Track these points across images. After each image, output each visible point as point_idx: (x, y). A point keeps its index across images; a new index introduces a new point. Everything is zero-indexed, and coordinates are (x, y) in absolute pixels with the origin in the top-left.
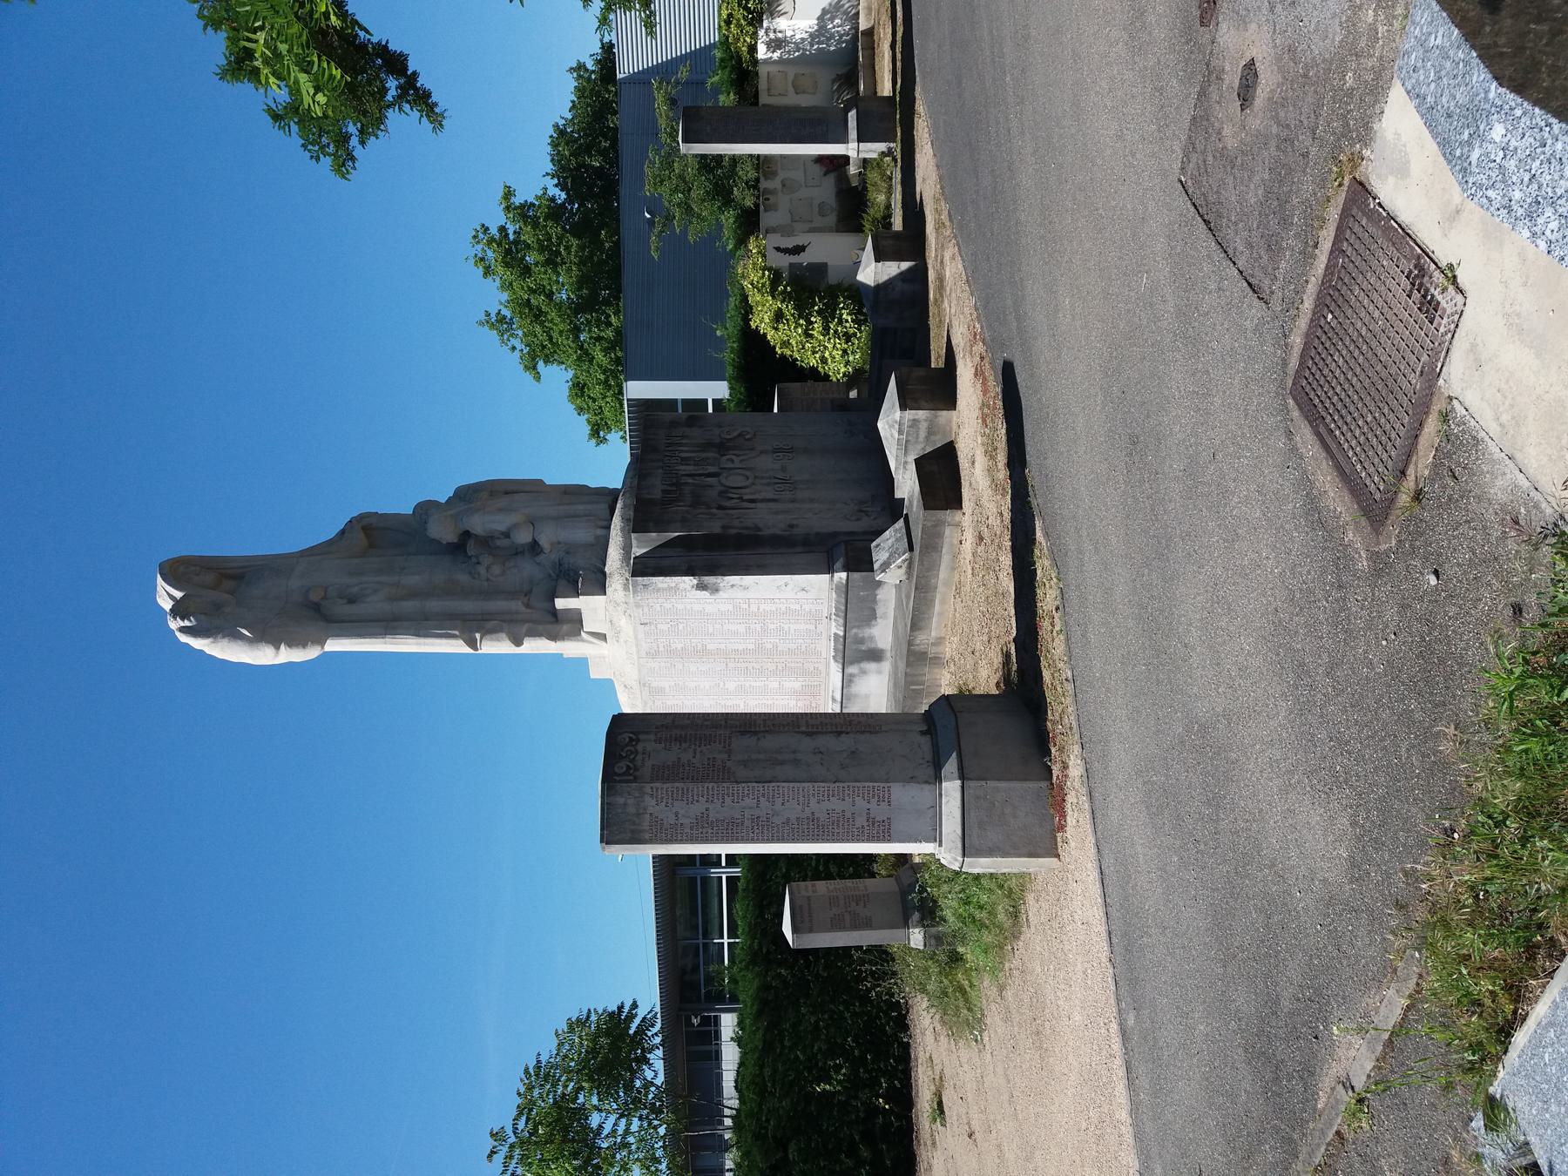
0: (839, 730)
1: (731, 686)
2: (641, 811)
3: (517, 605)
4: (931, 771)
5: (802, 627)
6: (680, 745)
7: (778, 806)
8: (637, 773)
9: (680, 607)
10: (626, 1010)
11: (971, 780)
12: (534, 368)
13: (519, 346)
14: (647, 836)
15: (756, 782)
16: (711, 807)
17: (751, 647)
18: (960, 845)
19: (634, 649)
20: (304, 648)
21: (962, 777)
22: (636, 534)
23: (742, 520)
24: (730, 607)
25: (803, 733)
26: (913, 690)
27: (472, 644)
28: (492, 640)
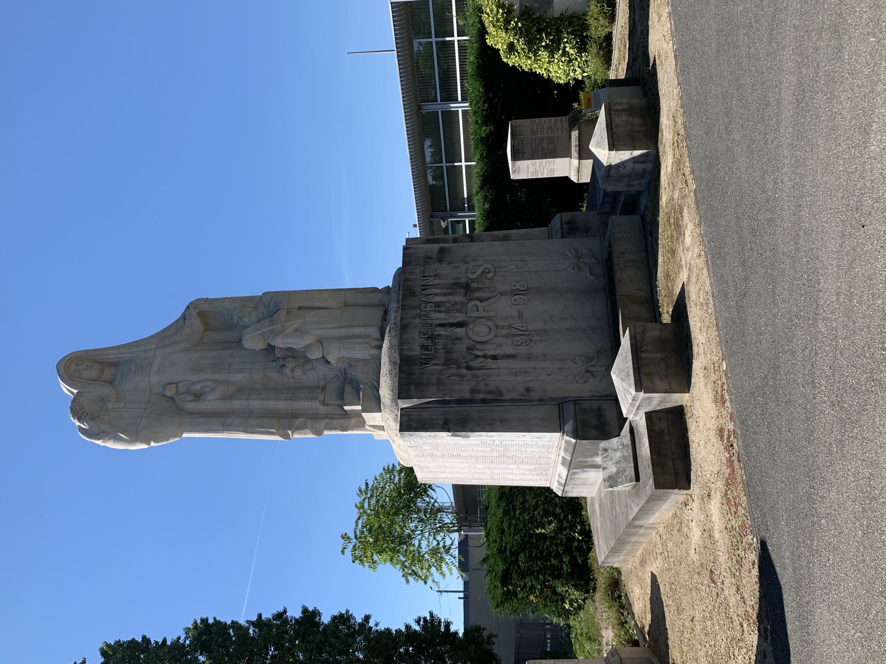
3: (315, 406)
22: (400, 400)
23: (487, 382)
27: (286, 436)
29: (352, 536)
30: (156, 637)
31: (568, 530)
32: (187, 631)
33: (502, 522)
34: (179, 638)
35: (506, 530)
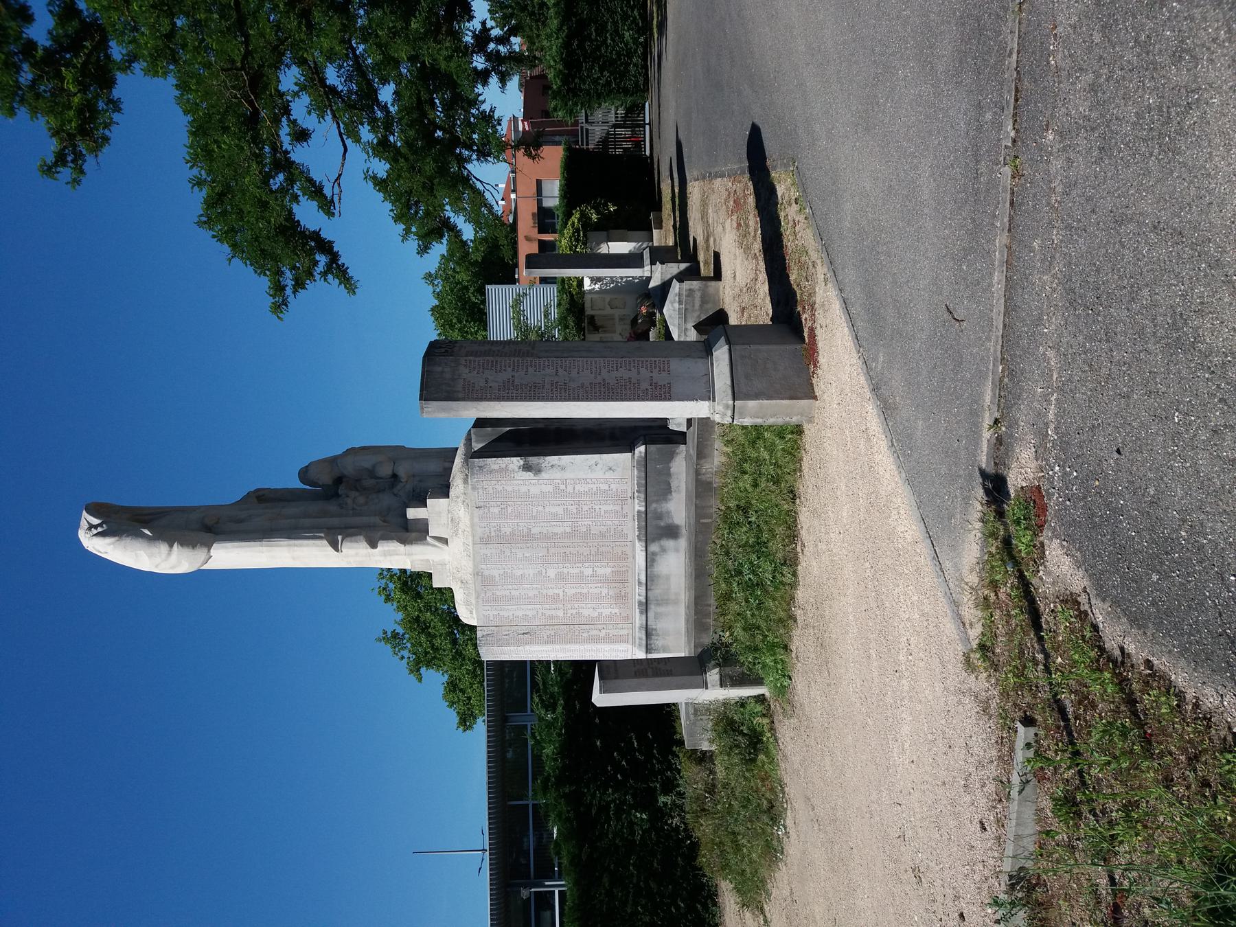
1: (552, 573)
2: (456, 377)
5: (610, 508)
7: (574, 374)
9: (509, 488)
12: (418, 670)
13: (406, 653)
14: (460, 395)
16: (516, 375)
17: (568, 530)
18: (730, 392)
19: (470, 538)
20: (193, 548)
24: (550, 488)
28: (351, 541)
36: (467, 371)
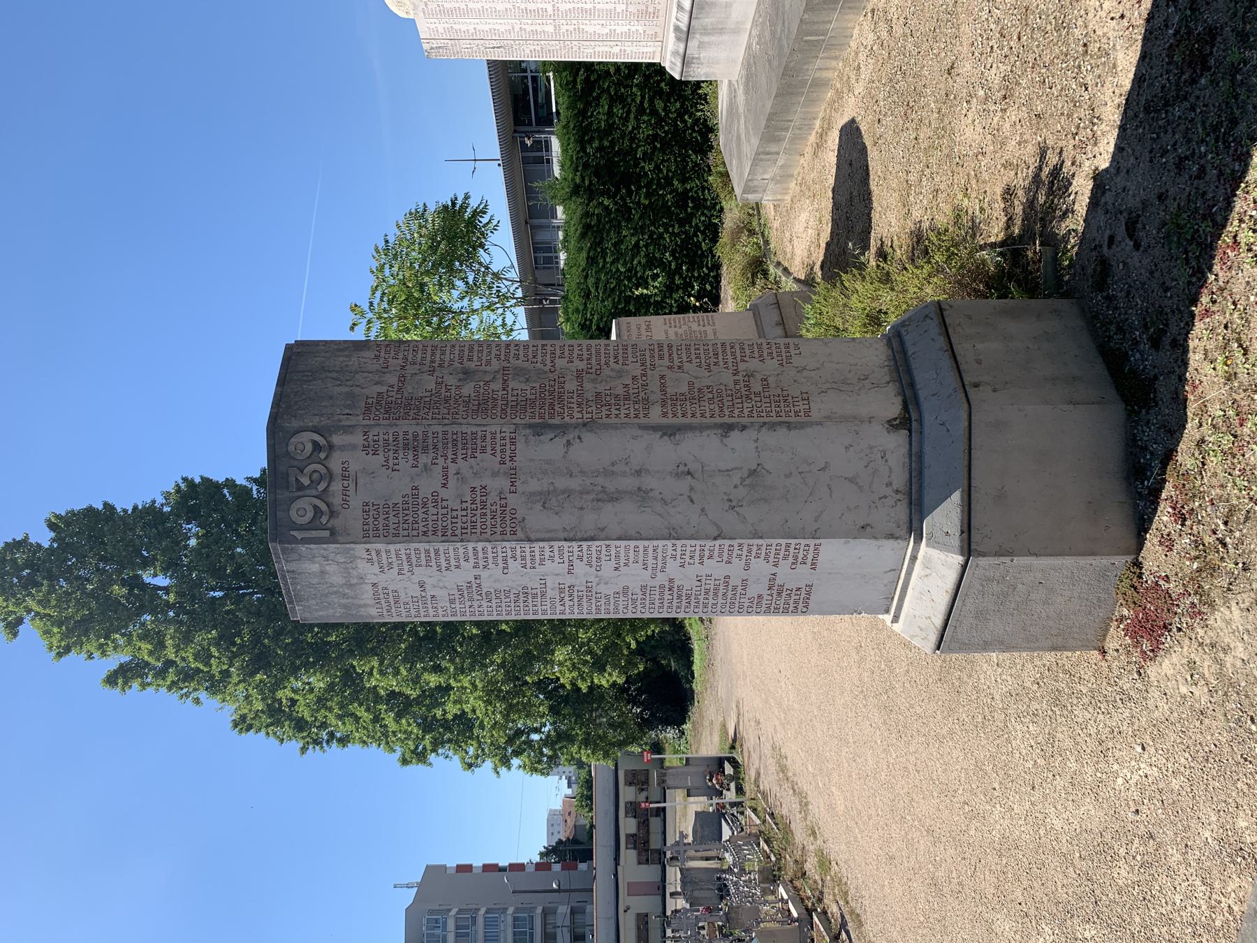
0: (727, 420)
2: (354, 581)
4: (901, 512)
6: (416, 457)
7: (608, 568)
8: (337, 522)
10: (459, 202)
11: (984, 555)
15: (566, 540)
16: (484, 574)
21: (968, 550)
25: (655, 428)
26: (806, 41)
29: (366, 307)
30: (124, 503)
31: (680, 292)
32: (167, 495)
33: (586, 277)
34: (154, 502)
35: (593, 290)
36: (376, 569)
